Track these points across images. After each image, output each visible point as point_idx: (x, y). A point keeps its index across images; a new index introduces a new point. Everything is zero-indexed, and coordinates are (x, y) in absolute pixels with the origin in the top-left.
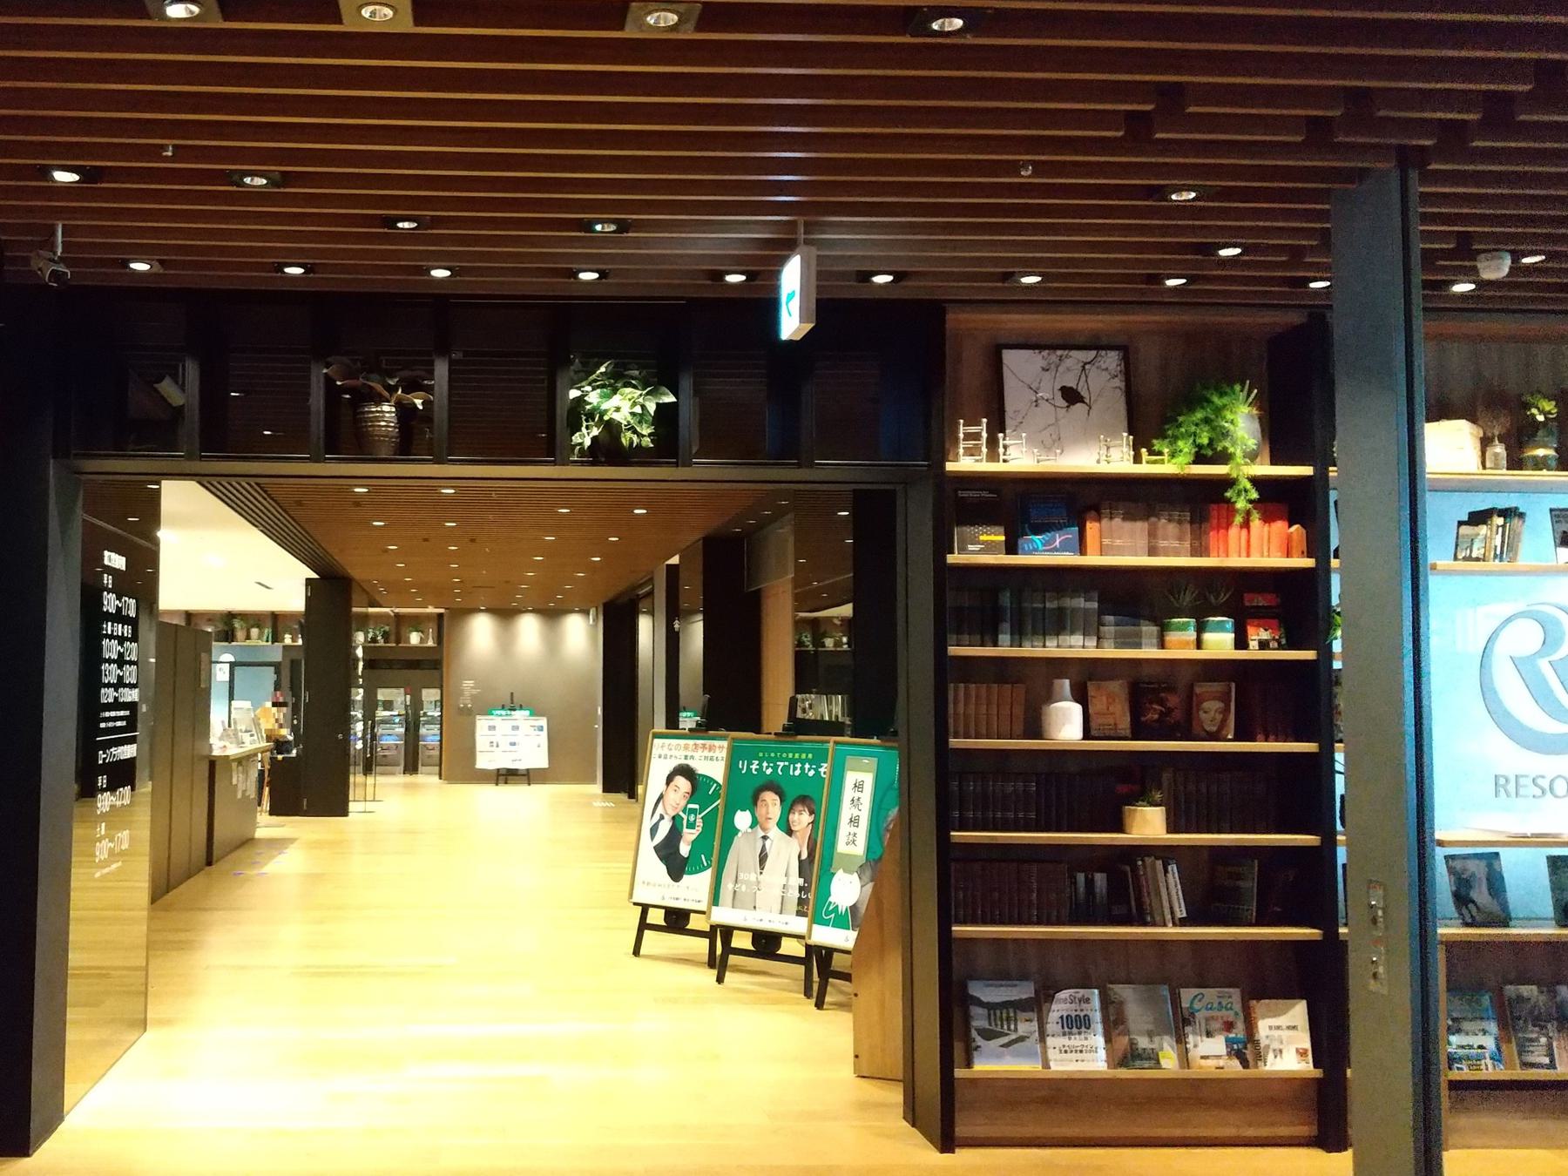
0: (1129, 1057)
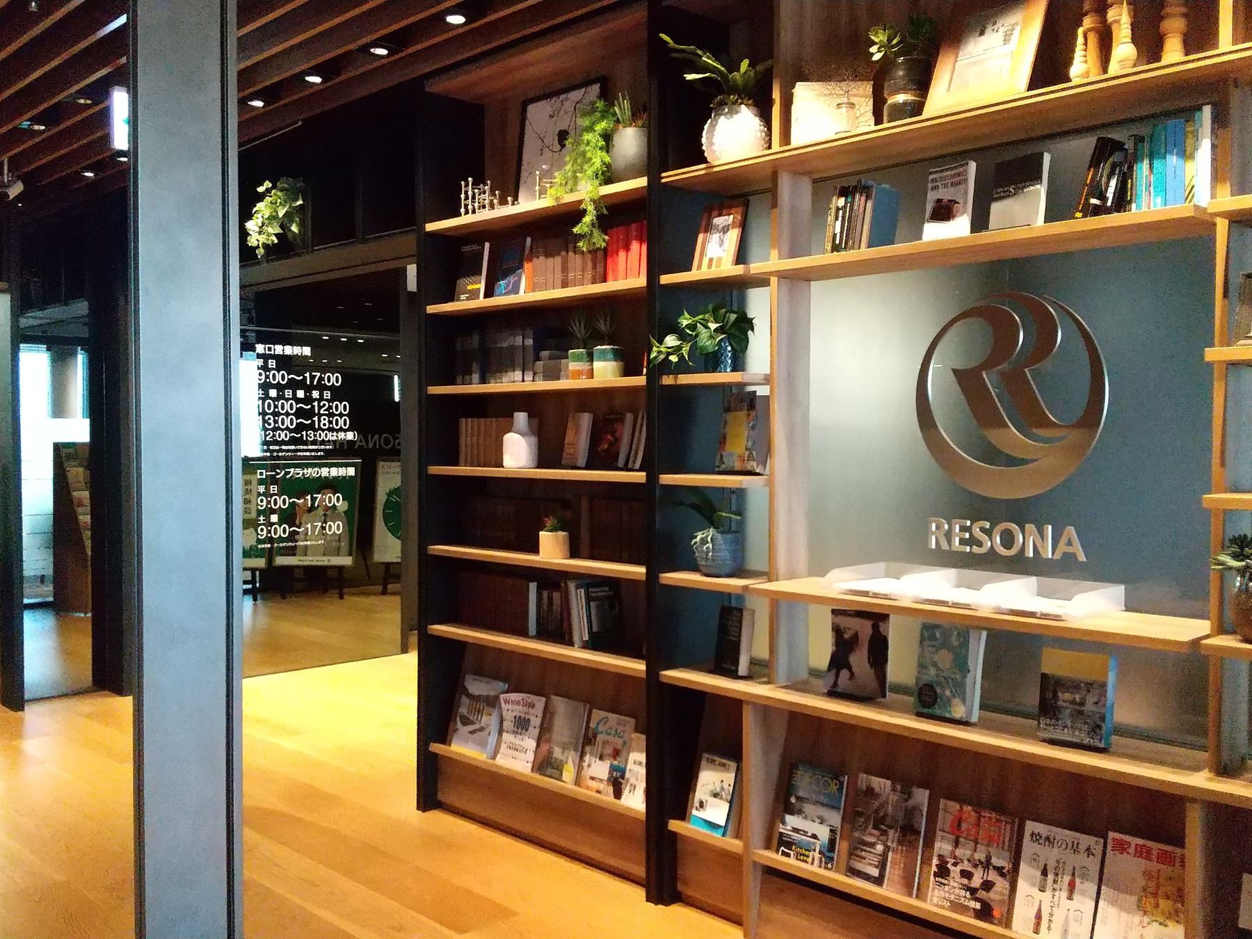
0: (545, 764)
